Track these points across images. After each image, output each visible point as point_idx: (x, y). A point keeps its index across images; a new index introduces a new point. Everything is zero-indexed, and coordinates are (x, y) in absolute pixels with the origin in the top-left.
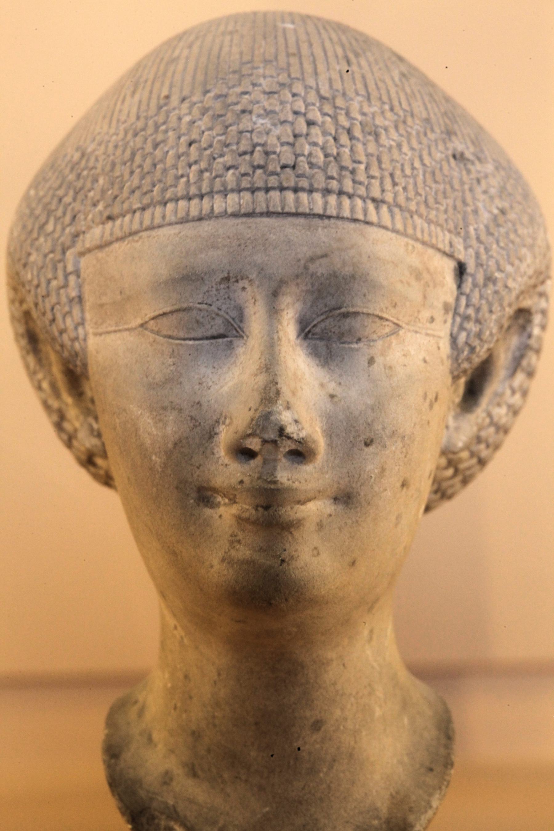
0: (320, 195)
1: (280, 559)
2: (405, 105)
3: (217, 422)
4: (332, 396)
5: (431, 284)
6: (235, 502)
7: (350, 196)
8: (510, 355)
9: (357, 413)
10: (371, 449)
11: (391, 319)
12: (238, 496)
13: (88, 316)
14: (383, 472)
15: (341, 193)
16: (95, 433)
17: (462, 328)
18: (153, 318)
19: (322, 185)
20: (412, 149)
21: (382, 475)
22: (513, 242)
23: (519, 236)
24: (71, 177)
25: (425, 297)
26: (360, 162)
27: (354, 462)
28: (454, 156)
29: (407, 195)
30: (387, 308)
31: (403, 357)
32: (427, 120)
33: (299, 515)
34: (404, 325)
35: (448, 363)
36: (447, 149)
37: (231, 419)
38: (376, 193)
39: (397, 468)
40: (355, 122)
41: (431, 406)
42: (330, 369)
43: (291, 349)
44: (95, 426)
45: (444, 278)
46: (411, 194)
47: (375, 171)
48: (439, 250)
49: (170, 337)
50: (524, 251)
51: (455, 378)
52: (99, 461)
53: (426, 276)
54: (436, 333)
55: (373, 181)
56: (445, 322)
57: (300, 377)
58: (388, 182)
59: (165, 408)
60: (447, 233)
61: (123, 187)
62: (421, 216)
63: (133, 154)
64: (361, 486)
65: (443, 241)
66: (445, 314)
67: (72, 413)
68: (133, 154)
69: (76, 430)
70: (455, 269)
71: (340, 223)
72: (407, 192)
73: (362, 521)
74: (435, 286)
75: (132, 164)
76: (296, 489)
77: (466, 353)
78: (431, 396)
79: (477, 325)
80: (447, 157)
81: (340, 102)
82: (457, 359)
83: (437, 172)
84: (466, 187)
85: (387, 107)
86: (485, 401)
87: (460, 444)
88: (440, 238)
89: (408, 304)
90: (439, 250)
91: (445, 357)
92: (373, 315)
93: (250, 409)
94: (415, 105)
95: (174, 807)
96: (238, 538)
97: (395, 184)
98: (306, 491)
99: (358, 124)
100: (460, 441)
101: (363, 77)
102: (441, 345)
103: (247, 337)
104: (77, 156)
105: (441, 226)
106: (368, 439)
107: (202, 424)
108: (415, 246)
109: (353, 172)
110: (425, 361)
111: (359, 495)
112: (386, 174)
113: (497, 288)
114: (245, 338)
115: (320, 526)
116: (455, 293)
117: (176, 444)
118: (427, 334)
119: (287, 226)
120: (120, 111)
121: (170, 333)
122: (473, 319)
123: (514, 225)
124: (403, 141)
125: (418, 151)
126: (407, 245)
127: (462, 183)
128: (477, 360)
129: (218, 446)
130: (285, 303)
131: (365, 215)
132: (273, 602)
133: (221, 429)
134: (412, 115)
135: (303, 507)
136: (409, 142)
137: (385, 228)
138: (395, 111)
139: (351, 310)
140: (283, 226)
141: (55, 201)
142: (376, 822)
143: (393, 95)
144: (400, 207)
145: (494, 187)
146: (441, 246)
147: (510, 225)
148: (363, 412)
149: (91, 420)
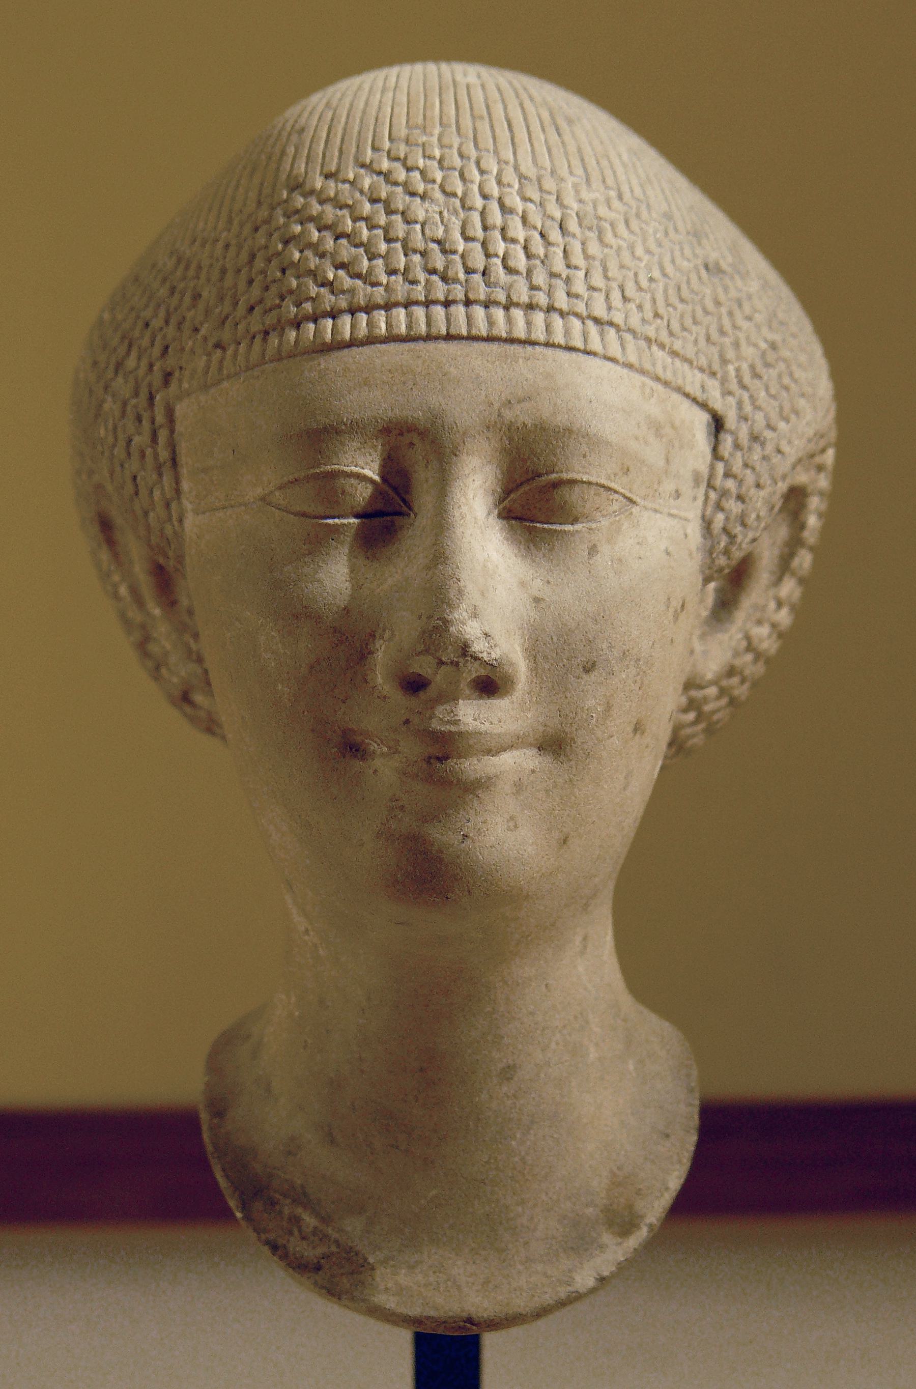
0: (522, 313)
1: (462, 833)
2: (638, 191)
3: (373, 636)
4: (537, 600)
5: (677, 444)
6: (397, 752)
7: (562, 314)
8: (776, 552)
9: (573, 625)
10: (593, 676)
11: (622, 491)
12: (402, 743)
13: (185, 486)
14: (609, 711)
15: (550, 309)
16: (194, 657)
17: (719, 507)
18: (280, 488)
19: (524, 299)
20: (648, 252)
21: (607, 714)
22: (787, 389)
23: (796, 381)
24: (163, 292)
25: (668, 461)
26: (576, 268)
27: (568, 695)
28: (706, 267)
29: (643, 316)
30: (615, 475)
31: (638, 547)
32: (668, 216)
33: (491, 771)
34: (638, 500)
35: (698, 557)
36: (696, 256)
37: (393, 631)
38: (600, 310)
39: (627, 705)
40: (569, 211)
41: (676, 617)
42: (534, 561)
43: (478, 532)
44: (194, 646)
45: (694, 436)
46: (649, 315)
47: (597, 280)
48: (687, 395)
49: (304, 515)
50: (802, 403)
51: (707, 580)
52: (198, 698)
53: (668, 430)
54: (682, 514)
55: (596, 294)
56: (695, 499)
57: (491, 572)
58: (616, 296)
59: (296, 617)
60: (696, 372)
61: (237, 303)
62: (662, 346)
63: (253, 256)
64: (576, 730)
65: (693, 383)
66: (694, 487)
67: (162, 630)
68: (253, 256)
69: (166, 654)
70: (709, 424)
71: (549, 352)
72: (642, 311)
73: (577, 780)
74: (681, 447)
75: (250, 270)
76: (486, 733)
77: (723, 544)
78: (676, 603)
79: (739, 503)
80: (696, 268)
81: (550, 184)
82: (711, 553)
83: (684, 287)
84: (724, 310)
85: (613, 194)
86: (740, 616)
87: (709, 676)
88: (689, 379)
89: (645, 469)
90: (687, 395)
91: (693, 547)
92: (597, 484)
93: (420, 617)
94: (650, 192)
95: (302, 1186)
96: (401, 803)
97: (625, 299)
98: (499, 735)
99: (574, 215)
100: (711, 668)
101: (580, 150)
102: (689, 531)
103: (416, 514)
104: (171, 264)
105: (690, 362)
106: (587, 663)
107: (350, 638)
108: (654, 388)
109: (568, 281)
110: (668, 553)
111: (575, 743)
112: (615, 285)
113: (767, 452)
114: (412, 515)
115: (519, 787)
116: (709, 457)
117: (312, 667)
118: (671, 515)
119: (474, 356)
120: (233, 199)
121: (305, 508)
122: (734, 496)
123: (788, 367)
124: (636, 241)
125: (657, 256)
126: (644, 385)
127: (718, 303)
128: (737, 555)
129: (374, 671)
130: (471, 466)
131: (586, 341)
132: (449, 895)
133: (378, 646)
134: (648, 206)
135: (494, 760)
136: (645, 241)
137: (613, 360)
138: (625, 200)
139: (565, 476)
140: (467, 355)
141: (140, 324)
142: (590, 1211)
143: (622, 178)
144: (633, 332)
145: (760, 312)
146: (688, 389)
147: (782, 366)
148: (581, 624)
149: (187, 638)
